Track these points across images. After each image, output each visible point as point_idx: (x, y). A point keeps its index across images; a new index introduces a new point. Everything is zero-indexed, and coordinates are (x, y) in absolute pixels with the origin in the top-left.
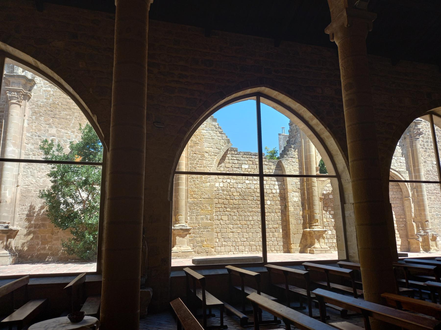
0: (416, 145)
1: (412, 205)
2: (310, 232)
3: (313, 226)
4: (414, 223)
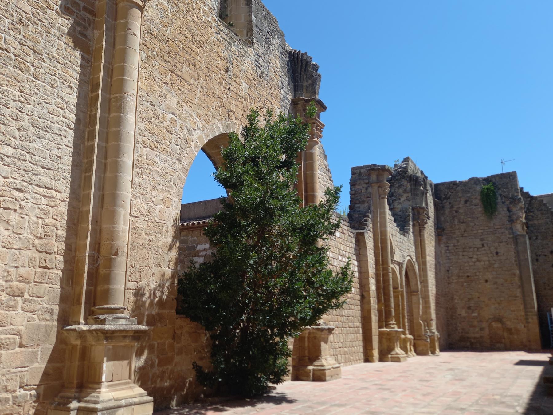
0: (423, 235)
1: (421, 301)
2: (389, 333)
3: (391, 324)
4: (421, 322)
